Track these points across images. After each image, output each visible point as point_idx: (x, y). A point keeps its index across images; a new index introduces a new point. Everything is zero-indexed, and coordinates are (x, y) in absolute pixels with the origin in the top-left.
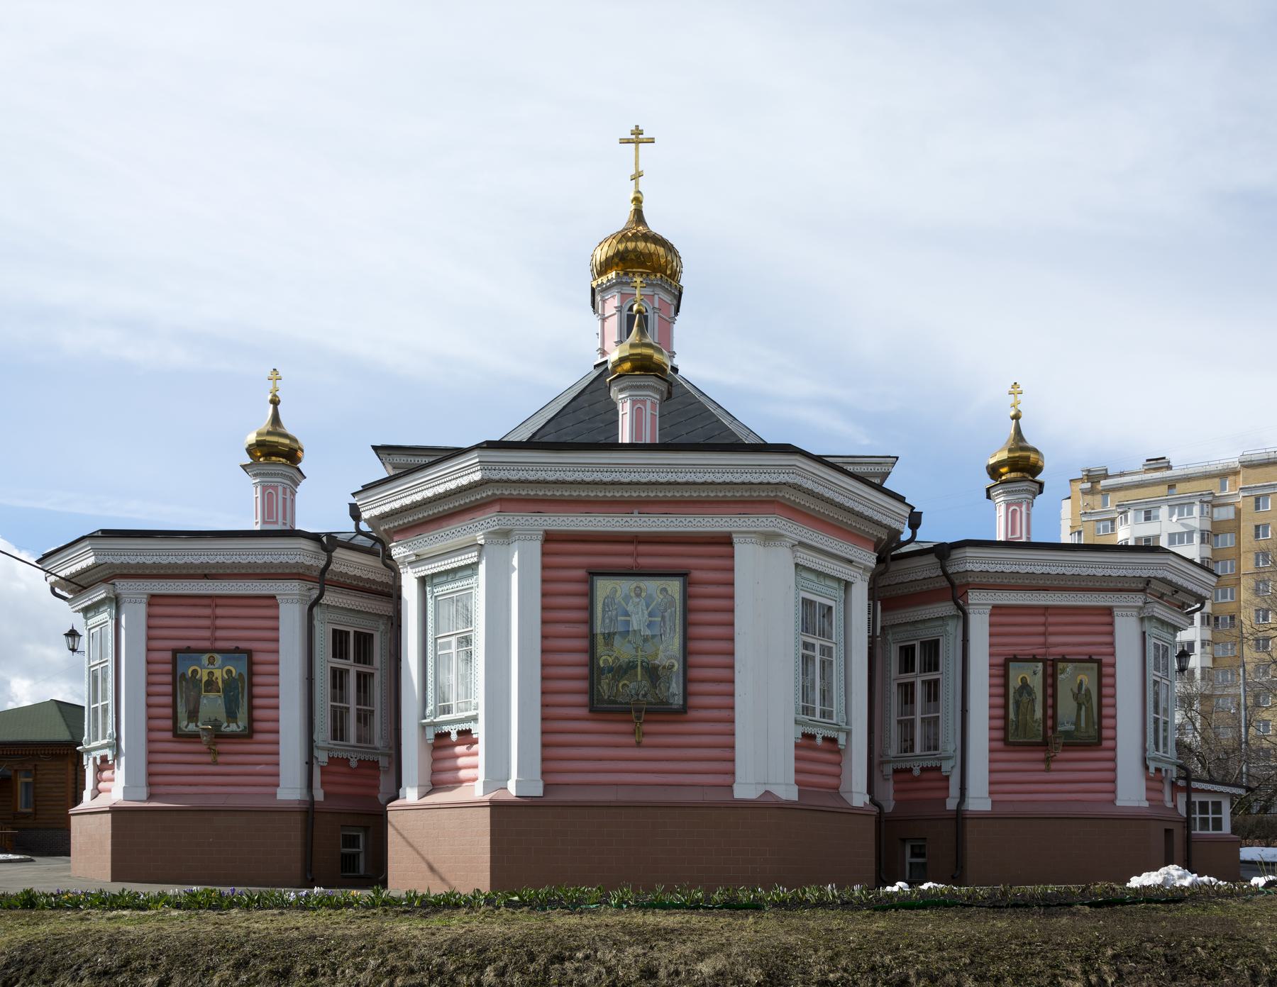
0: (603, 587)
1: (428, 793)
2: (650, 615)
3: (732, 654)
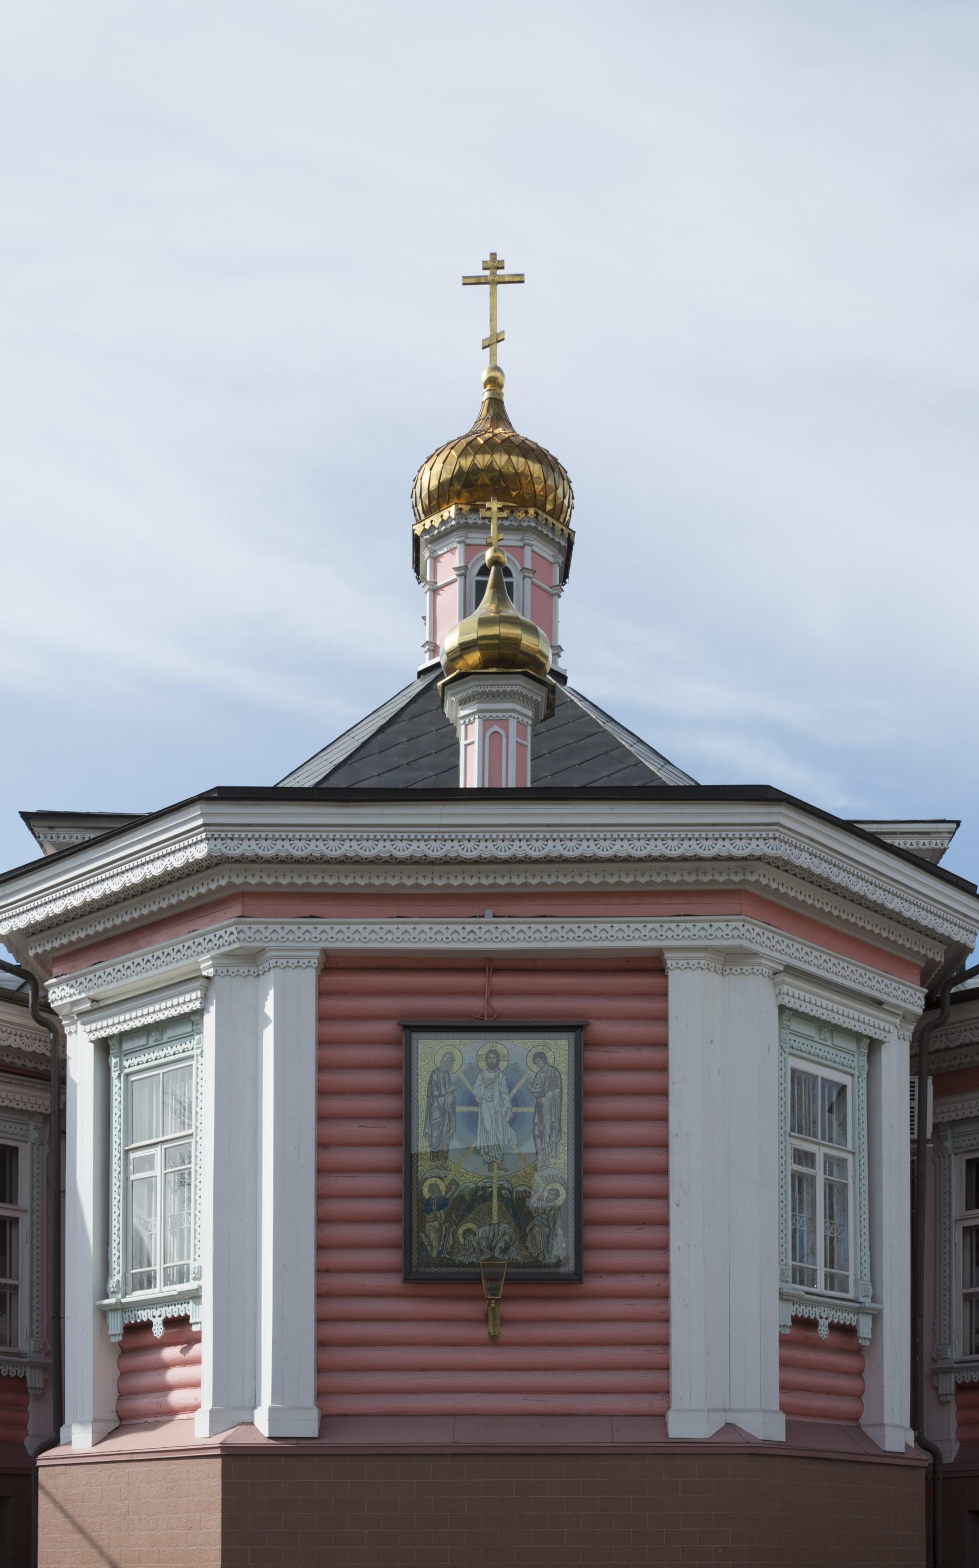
0: (431, 1052)
1: (111, 1435)
2: (515, 1102)
3: (664, 1172)
